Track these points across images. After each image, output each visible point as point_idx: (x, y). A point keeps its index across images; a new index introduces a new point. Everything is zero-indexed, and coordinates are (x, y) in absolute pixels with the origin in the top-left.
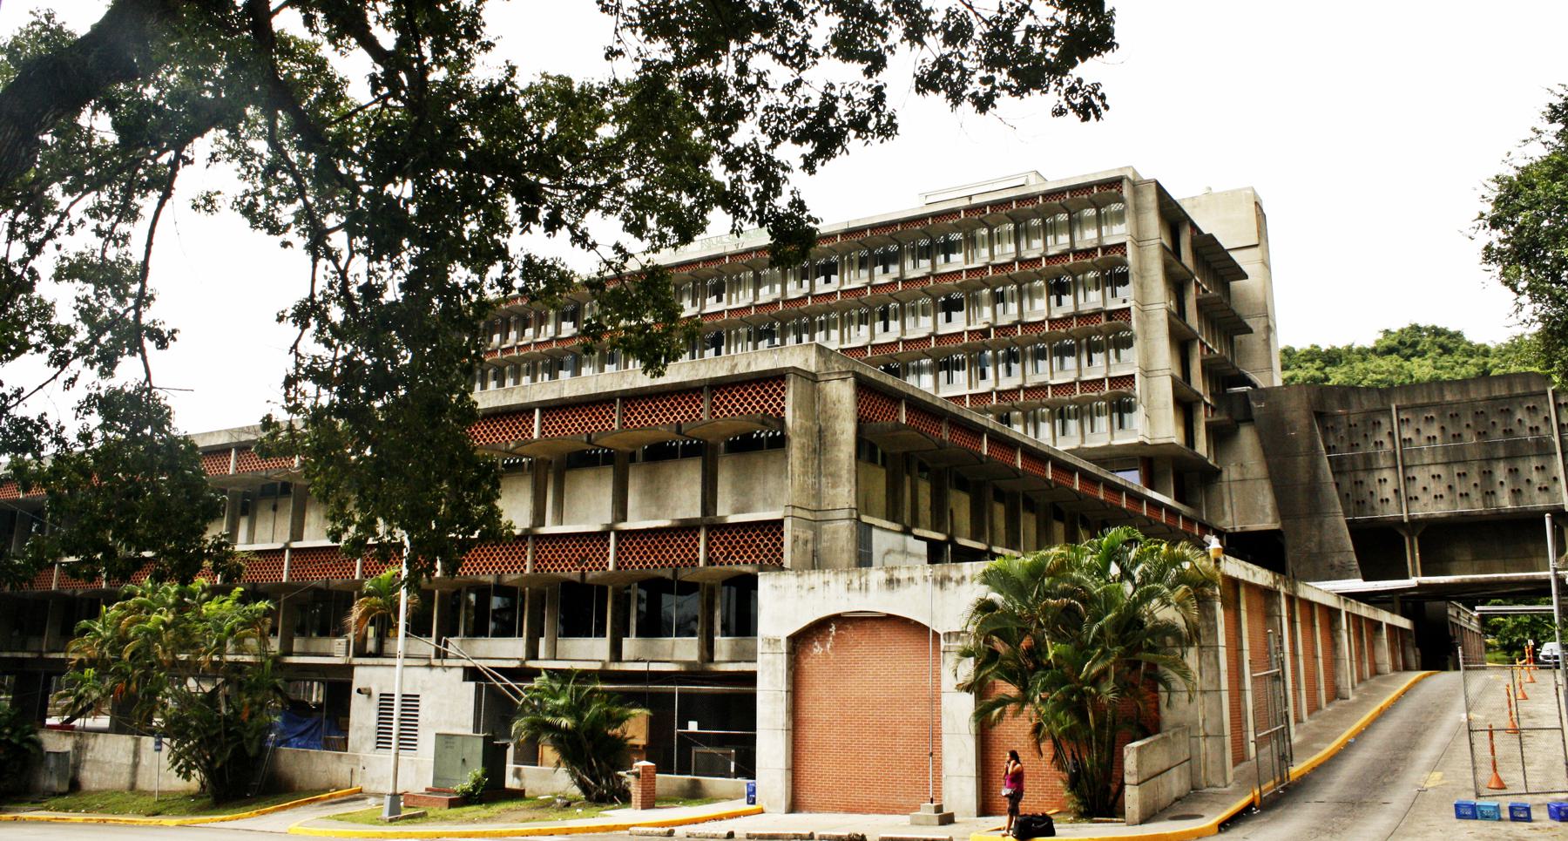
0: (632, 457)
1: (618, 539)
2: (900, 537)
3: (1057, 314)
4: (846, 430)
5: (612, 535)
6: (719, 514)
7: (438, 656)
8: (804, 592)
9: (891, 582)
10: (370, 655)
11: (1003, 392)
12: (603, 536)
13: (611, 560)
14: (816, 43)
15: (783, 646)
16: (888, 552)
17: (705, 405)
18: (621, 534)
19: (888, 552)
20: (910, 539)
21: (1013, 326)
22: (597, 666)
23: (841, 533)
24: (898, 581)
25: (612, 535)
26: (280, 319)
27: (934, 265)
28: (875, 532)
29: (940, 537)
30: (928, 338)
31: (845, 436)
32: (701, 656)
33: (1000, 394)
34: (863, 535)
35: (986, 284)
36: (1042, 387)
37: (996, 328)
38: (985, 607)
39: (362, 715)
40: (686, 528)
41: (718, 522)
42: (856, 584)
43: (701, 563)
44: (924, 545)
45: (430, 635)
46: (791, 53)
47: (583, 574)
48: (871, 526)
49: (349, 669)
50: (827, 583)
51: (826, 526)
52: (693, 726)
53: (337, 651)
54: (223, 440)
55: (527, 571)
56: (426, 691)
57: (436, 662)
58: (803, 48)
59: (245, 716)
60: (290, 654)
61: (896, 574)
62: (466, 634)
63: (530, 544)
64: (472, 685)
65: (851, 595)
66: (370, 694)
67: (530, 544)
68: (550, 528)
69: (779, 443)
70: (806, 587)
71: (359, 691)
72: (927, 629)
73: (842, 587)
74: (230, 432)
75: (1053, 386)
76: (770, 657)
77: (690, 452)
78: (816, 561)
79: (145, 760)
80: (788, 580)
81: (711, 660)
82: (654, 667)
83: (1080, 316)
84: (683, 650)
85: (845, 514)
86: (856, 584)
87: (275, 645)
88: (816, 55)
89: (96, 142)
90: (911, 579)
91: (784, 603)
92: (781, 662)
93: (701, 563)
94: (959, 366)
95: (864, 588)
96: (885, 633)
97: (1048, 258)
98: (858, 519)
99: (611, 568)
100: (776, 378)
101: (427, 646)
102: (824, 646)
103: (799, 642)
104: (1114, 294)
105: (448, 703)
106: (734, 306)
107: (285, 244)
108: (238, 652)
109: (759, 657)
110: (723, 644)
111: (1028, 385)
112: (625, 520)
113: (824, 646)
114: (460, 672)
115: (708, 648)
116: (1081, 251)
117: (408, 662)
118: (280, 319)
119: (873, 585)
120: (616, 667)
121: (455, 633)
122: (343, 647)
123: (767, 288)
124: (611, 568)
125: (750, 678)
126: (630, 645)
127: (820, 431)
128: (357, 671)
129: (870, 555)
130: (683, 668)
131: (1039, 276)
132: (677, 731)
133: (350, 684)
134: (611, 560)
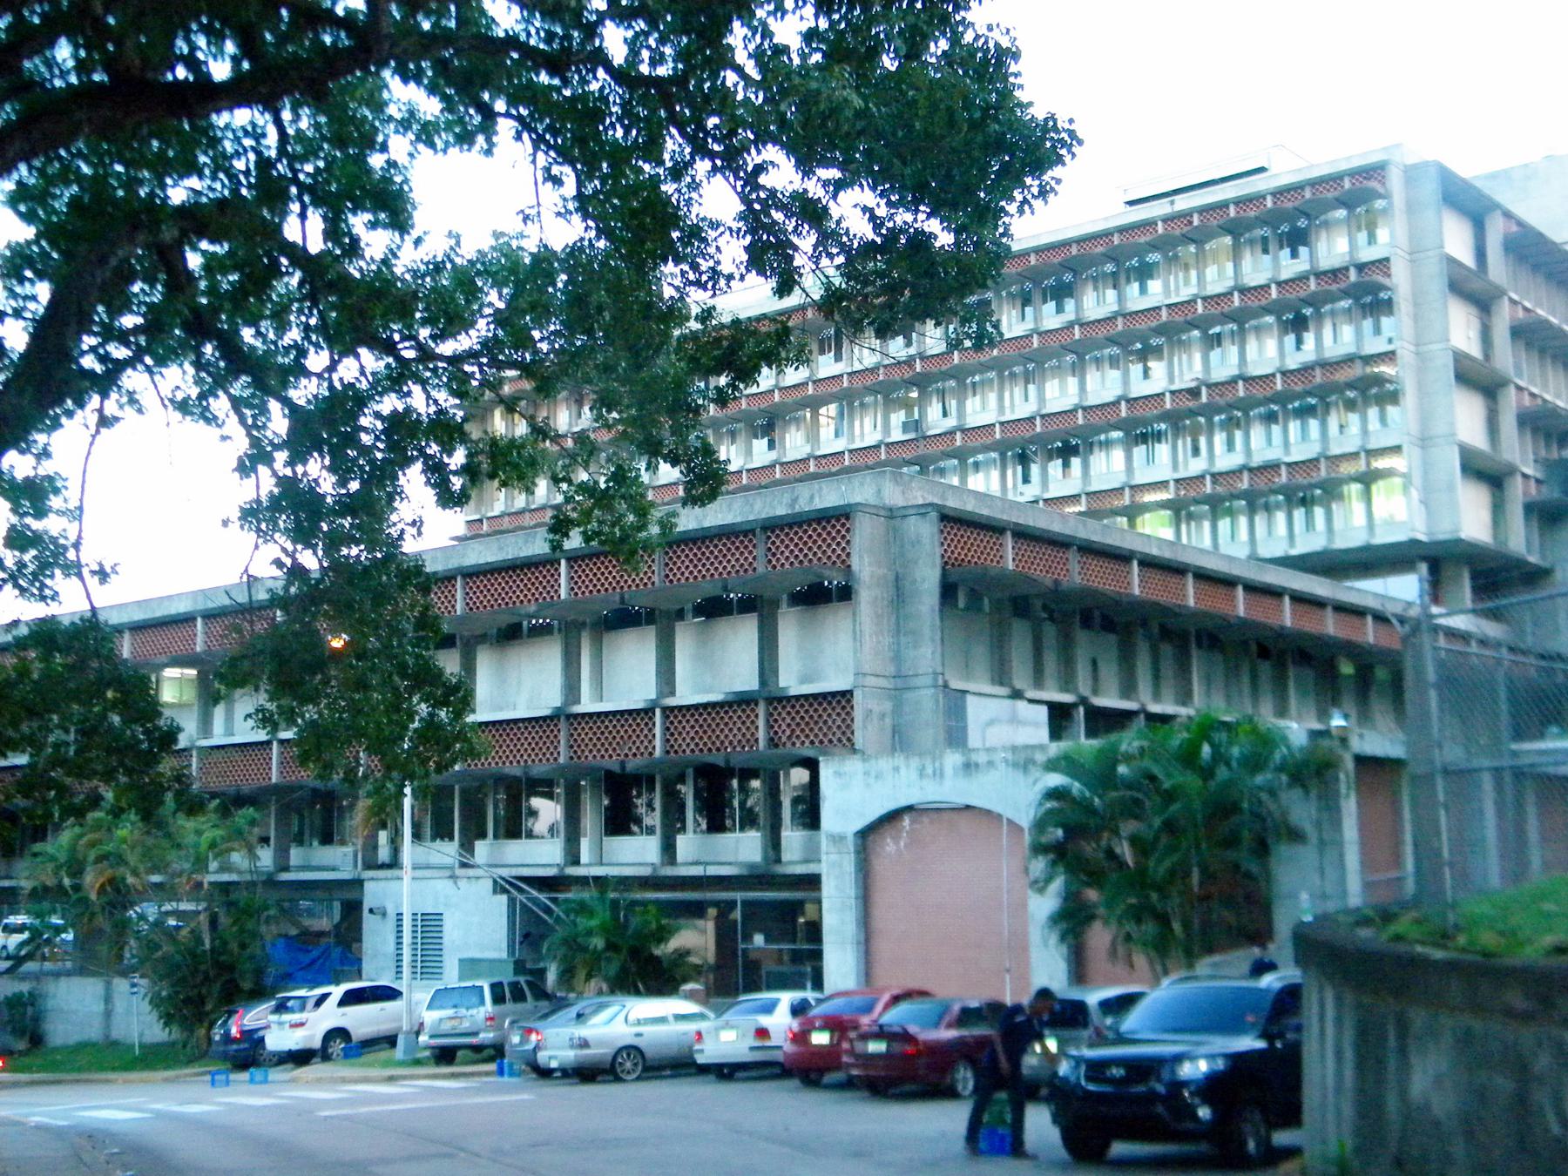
0: (680, 615)
1: (665, 717)
2: (1008, 702)
3: (1293, 362)
4: (928, 578)
5: (658, 712)
6: (782, 684)
7: (464, 865)
8: (872, 780)
9: (969, 767)
10: (383, 866)
11: (1220, 474)
12: (648, 712)
13: (658, 742)
14: (726, 268)
15: (850, 840)
16: (991, 723)
17: (760, 552)
18: (668, 711)
19: (991, 723)
20: (1021, 705)
21: (1232, 382)
22: (645, 872)
23: (926, 700)
24: (977, 765)
25: (658, 712)
26: (225, 523)
27: (1121, 299)
28: (970, 699)
29: (1067, 698)
30: (1116, 403)
31: (926, 586)
32: (765, 858)
33: (1216, 477)
34: (955, 703)
35: (1192, 325)
36: (1272, 467)
37: (1209, 386)
38: (1055, 794)
39: (377, 939)
40: (743, 701)
41: (779, 694)
42: (929, 771)
43: (762, 743)
44: (1044, 710)
45: (451, 838)
46: (704, 278)
47: (623, 763)
48: (965, 692)
49: (358, 883)
50: (896, 769)
51: (908, 695)
52: (759, 939)
53: (337, 861)
54: (182, 607)
55: (561, 760)
56: (443, 904)
57: (460, 872)
58: (715, 274)
59: (234, 946)
60: (286, 869)
61: (974, 757)
62: (496, 837)
63: (563, 725)
64: (504, 898)
65: (925, 782)
66: (384, 914)
67: (563, 725)
68: (587, 705)
69: (845, 593)
70: (873, 774)
71: (371, 911)
72: (1000, 816)
73: (914, 775)
74: (194, 594)
75: (1289, 465)
76: (833, 857)
77: (748, 605)
78: (900, 740)
79: (119, 1005)
80: (853, 765)
81: (778, 860)
82: (712, 871)
83: (1325, 365)
84: (741, 848)
85: (928, 680)
86: (929, 771)
87: (266, 857)
88: (730, 277)
89: (58, 572)
90: (990, 763)
91: (852, 792)
92: (849, 863)
93: (762, 743)
94: (1159, 437)
95: (939, 774)
96: (963, 821)
97: (1279, 284)
98: (946, 686)
99: (658, 753)
100: (839, 517)
101: (448, 851)
102: (897, 843)
103: (868, 834)
104: (1377, 330)
105: (477, 924)
106: (857, 367)
107: (224, 438)
108: (222, 870)
109: (824, 857)
110: (792, 838)
111: (1254, 465)
112: (673, 693)
113: (897, 843)
114: (490, 883)
115: (774, 843)
116: (1325, 273)
117: (419, 873)
118: (225, 523)
119: (949, 770)
120: (669, 871)
121: (482, 835)
122: (350, 858)
123: (900, 340)
124: (658, 753)
125: (812, 882)
126: (687, 844)
127: (897, 579)
128: (368, 886)
129: (965, 728)
130: (744, 872)
131: (1267, 310)
132: (741, 946)
133: (361, 903)
134: (658, 742)
